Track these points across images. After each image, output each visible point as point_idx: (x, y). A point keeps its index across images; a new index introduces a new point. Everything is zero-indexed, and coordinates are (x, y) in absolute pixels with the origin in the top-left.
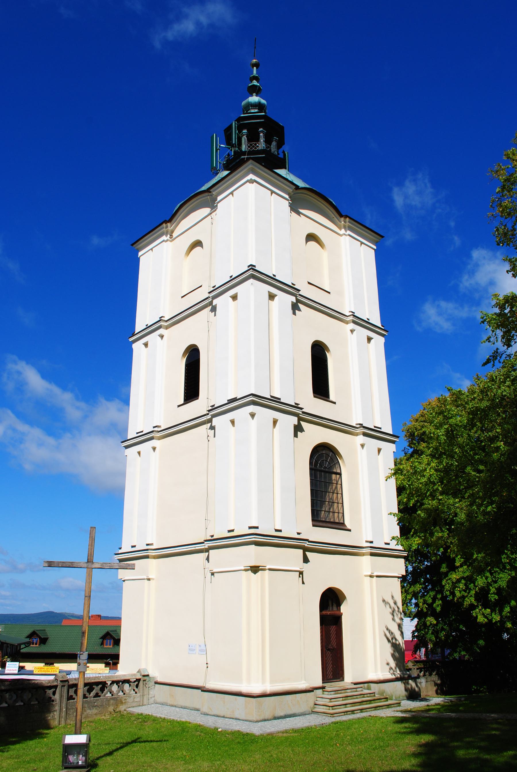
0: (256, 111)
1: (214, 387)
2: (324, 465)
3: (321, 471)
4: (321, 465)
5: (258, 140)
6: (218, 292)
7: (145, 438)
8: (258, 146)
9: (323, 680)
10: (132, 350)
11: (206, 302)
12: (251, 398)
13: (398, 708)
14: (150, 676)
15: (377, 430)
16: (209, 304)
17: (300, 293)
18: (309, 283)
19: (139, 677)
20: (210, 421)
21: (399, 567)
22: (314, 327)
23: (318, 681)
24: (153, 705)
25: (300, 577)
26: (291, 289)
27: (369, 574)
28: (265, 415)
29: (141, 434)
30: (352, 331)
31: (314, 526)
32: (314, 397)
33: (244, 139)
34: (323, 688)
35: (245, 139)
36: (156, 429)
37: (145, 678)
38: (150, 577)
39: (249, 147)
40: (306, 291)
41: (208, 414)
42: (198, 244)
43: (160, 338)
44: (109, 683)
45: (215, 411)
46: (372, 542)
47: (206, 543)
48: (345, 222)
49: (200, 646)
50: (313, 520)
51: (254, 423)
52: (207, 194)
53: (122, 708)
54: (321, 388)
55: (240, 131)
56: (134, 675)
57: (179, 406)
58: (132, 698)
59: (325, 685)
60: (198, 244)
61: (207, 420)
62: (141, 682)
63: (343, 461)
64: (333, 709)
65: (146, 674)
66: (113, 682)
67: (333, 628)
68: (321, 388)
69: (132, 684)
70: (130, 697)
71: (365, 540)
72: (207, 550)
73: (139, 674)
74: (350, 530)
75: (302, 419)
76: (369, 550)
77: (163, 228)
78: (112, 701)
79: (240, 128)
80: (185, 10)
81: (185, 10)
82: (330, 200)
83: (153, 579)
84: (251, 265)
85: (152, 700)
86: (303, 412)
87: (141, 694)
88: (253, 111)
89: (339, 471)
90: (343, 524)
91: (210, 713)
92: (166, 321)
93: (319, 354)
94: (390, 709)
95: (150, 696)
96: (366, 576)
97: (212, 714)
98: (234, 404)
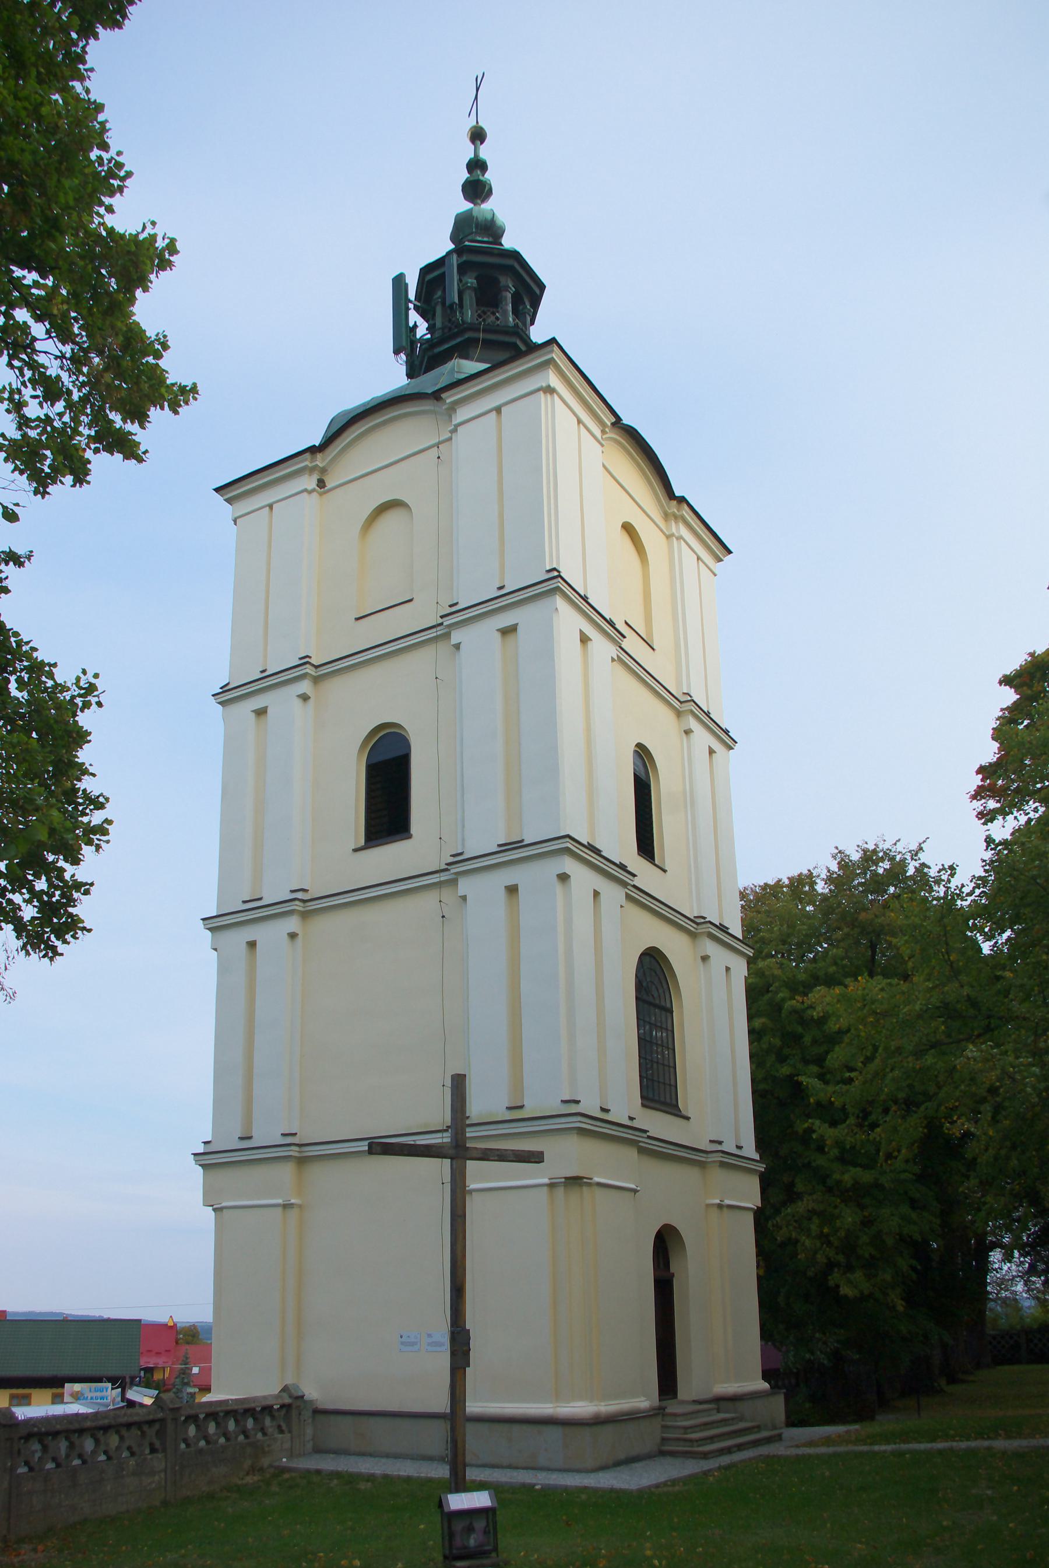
0: (485, 239)
12: (569, 844)
16: (439, 633)
17: (637, 882)
27: (718, 1201)
31: (643, 1105)
33: (469, 298)
36: (299, 895)
38: (293, 1201)
41: (446, 870)
44: (202, 1416)
49: (429, 1336)
50: (642, 1097)
53: (265, 1462)
54: (646, 845)
57: (355, 850)
59: (664, 1403)
62: (294, 1413)
65: (300, 1394)
68: (646, 845)
69: (276, 1414)
73: (285, 1395)
76: (718, 1157)
79: (463, 269)
80: (100, 30)
81: (100, 30)
86: (649, 1137)
90: (677, 1106)
92: (316, 667)
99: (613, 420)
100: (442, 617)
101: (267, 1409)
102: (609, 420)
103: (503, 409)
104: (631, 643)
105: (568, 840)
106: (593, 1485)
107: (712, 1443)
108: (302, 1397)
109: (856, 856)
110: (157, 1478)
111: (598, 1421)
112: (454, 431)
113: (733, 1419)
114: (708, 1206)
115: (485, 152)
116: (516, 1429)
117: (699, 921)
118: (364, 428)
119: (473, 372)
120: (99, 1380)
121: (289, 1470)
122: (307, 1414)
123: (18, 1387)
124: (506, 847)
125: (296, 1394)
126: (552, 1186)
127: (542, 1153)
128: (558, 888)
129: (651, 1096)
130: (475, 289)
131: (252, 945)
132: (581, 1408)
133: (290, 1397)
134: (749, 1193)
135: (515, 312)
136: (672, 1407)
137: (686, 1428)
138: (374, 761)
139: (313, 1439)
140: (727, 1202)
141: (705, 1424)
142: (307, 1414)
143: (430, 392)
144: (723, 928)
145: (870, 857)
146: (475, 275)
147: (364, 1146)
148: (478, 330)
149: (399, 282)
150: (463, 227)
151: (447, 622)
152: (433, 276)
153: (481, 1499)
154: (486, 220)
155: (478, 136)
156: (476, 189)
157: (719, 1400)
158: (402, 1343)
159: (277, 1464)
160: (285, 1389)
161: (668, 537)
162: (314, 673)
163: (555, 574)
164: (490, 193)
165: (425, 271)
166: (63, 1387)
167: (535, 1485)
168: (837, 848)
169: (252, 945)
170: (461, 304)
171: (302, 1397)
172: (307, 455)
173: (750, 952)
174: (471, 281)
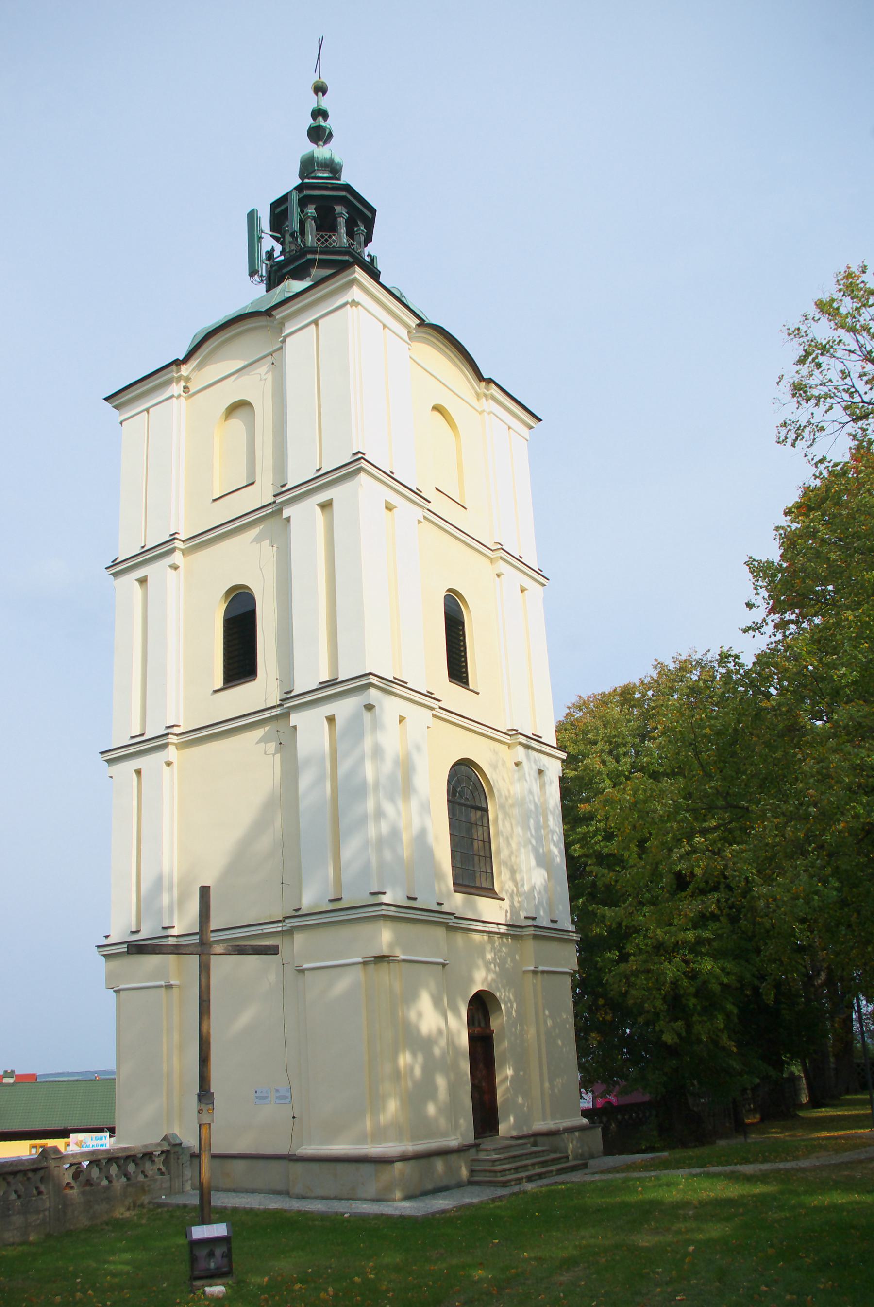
0: (326, 175)
3: (461, 804)
4: (461, 796)
5: (332, 228)
8: (334, 241)
10: (788, 585)
11: (269, 510)
13: (587, 1171)
23: (471, 1139)
27: (532, 968)
33: (310, 225)
34: (476, 1145)
35: (311, 225)
37: (177, 1149)
38: (172, 982)
39: (319, 240)
45: (291, 701)
46: (534, 919)
47: (287, 921)
49: (277, 1091)
54: (458, 671)
57: (216, 691)
58: (158, 1183)
59: (478, 1141)
61: (279, 716)
64: (502, 1176)
65: (178, 1142)
68: (458, 671)
69: (156, 1159)
76: (531, 931)
77: (173, 371)
79: (303, 203)
84: (359, 452)
86: (456, 917)
88: (320, 175)
89: (484, 806)
90: (493, 889)
92: (183, 541)
99: (418, 322)
100: (275, 496)
101: (148, 1156)
102: (413, 322)
103: (320, 322)
104: (439, 505)
105: (371, 676)
106: (390, 1212)
107: (517, 1173)
108: (181, 1144)
109: (672, 666)
110: (41, 1216)
112: (284, 341)
113: (543, 1151)
114: (525, 972)
115: (325, 103)
116: (340, 1166)
117: (513, 733)
118: (223, 338)
119: (298, 291)
120: (101, 1130)
121: (167, 1205)
122: (185, 1158)
123: (35, 1139)
124: (324, 685)
125: (174, 1142)
126: (365, 963)
127: (277, 947)
128: (367, 716)
129: (461, 882)
130: (314, 218)
131: (138, 772)
133: (169, 1145)
134: (567, 959)
135: (350, 234)
136: (488, 1143)
137: (495, 1161)
138: (229, 617)
139: (191, 1179)
140: (541, 968)
141: (514, 1157)
142: (185, 1158)
143: (263, 310)
144: (537, 739)
145: (684, 667)
146: (314, 206)
147: (124, 948)
148: (315, 253)
149: (252, 217)
150: (308, 166)
151: (279, 500)
152: (280, 210)
153: (219, 1230)
154: (325, 159)
156: (318, 135)
157: (537, 1136)
158: (257, 1097)
159: (156, 1200)
160: (165, 1138)
161: (481, 413)
163: (359, 456)
164: (330, 135)
165: (274, 205)
166: (69, 1137)
167: (345, 1213)
168: (656, 660)
170: (303, 231)
171: (181, 1144)
172: (174, 367)
173: (564, 756)
174: (311, 210)
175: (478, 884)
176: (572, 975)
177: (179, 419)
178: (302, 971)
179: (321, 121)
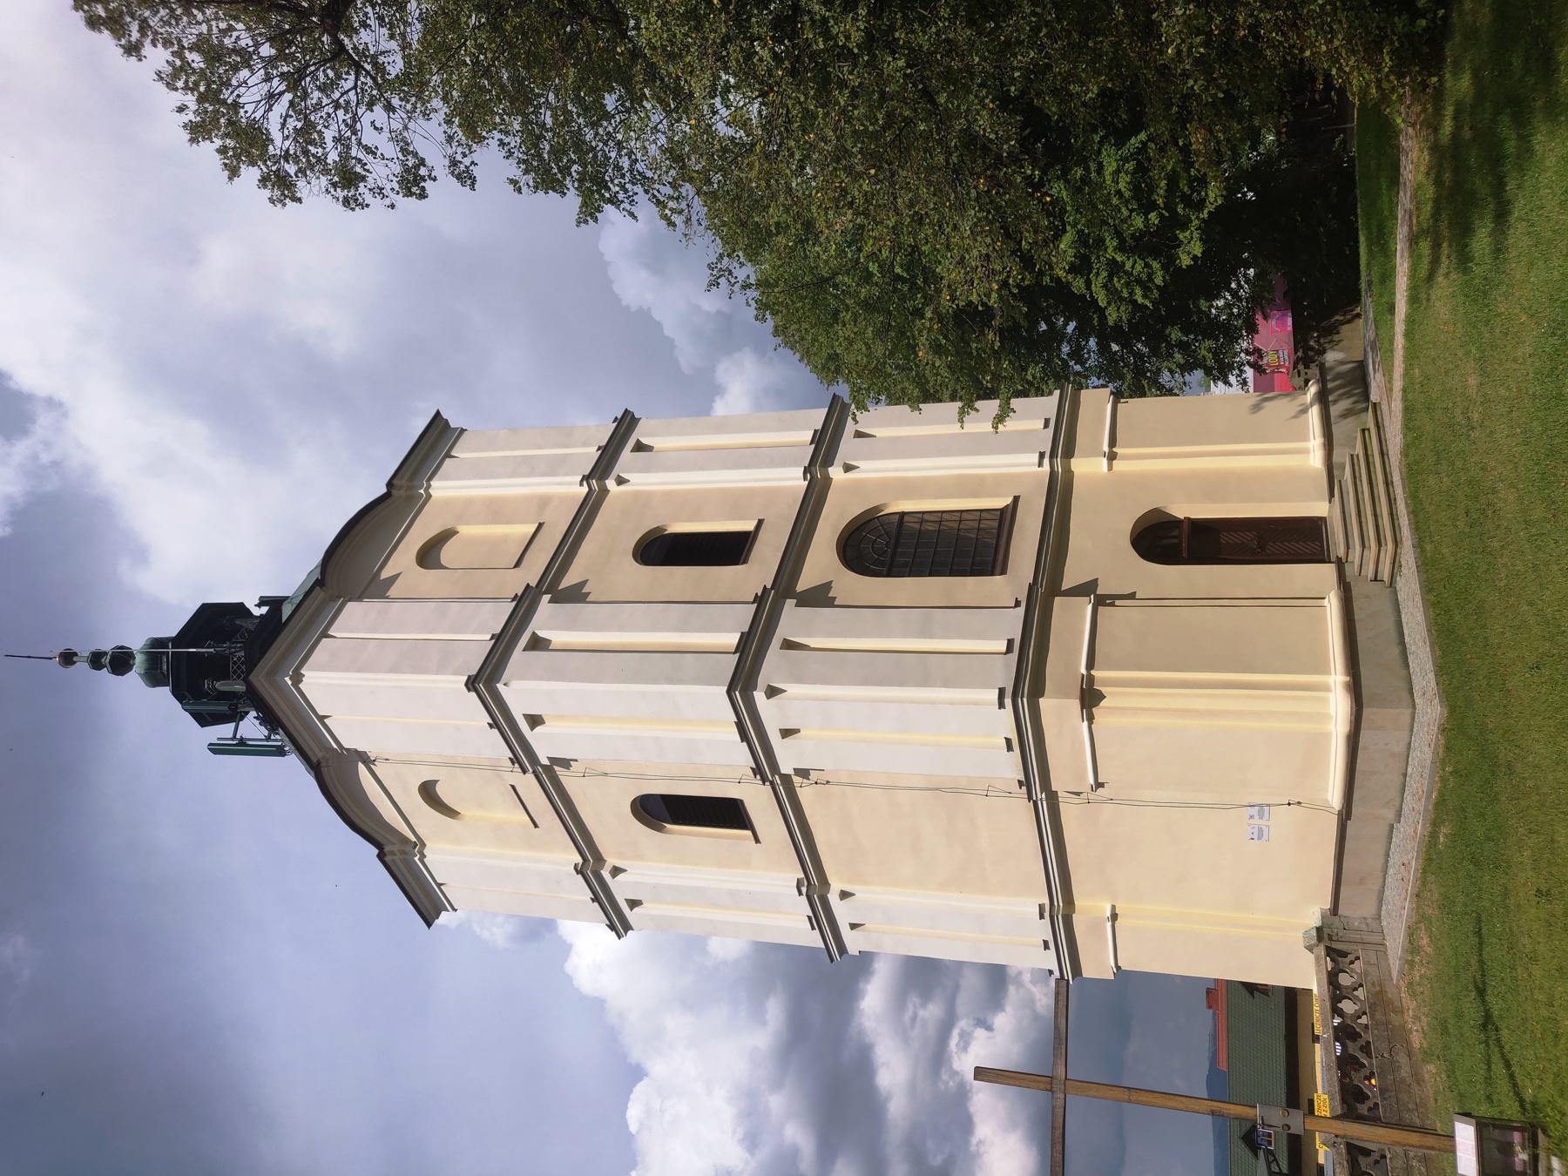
1: (721, 766)
2: (893, 546)
6: (523, 755)
7: (822, 916)
9: (1323, 561)
13: (1385, 407)
14: (1319, 924)
15: (818, 439)
16: (550, 775)
18: (517, 565)
19: (1321, 950)
20: (786, 779)
21: (1096, 402)
22: (606, 556)
23: (1327, 571)
24: (1394, 915)
25: (1112, 605)
26: (525, 604)
27: (1105, 461)
28: (774, 664)
29: (814, 921)
30: (621, 481)
31: (1003, 572)
32: (745, 562)
33: (221, 686)
34: (1340, 565)
36: (804, 890)
40: (532, 573)
42: (428, 792)
43: (621, 877)
45: (765, 767)
48: (401, 487)
51: (792, 689)
52: (324, 770)
55: (206, 695)
56: (1317, 959)
57: (757, 840)
58: (1370, 969)
60: (428, 792)
63: (885, 505)
65: (1314, 933)
66: (1336, 1011)
67: (1225, 538)
68: (726, 549)
70: (1367, 974)
71: (1036, 469)
72: (1052, 798)
74: (1016, 499)
75: (784, 586)
78: (1378, 1016)
82: (1362, 239)
83: (1114, 907)
85: (1374, 925)
87: (1359, 947)
90: (1003, 511)
91: (1397, 804)
93: (663, 549)
94: (1387, 423)
95: (1364, 927)
96: (1110, 468)
97: (1398, 800)
98: (750, 728)
102: (319, 594)
111: (1355, 689)
115: (85, 651)
124: (744, 736)
131: (853, 926)
132: (1338, 705)
140: (1106, 449)
149: (216, 749)
150: (154, 677)
155: (68, 658)
160: (1310, 948)
162: (592, 866)
165: (204, 720)
169: (853, 926)
175: (996, 524)
176: (1118, 396)
177: (445, 856)
178: (1099, 785)
179: (106, 660)
